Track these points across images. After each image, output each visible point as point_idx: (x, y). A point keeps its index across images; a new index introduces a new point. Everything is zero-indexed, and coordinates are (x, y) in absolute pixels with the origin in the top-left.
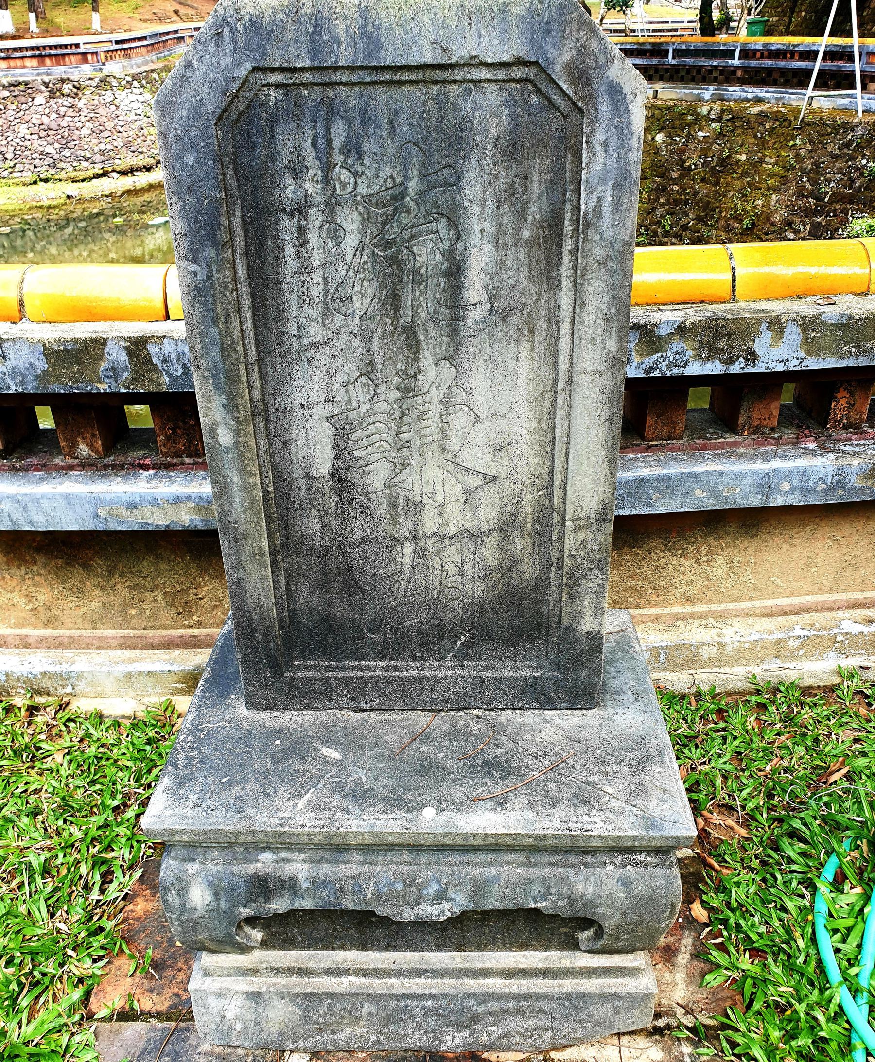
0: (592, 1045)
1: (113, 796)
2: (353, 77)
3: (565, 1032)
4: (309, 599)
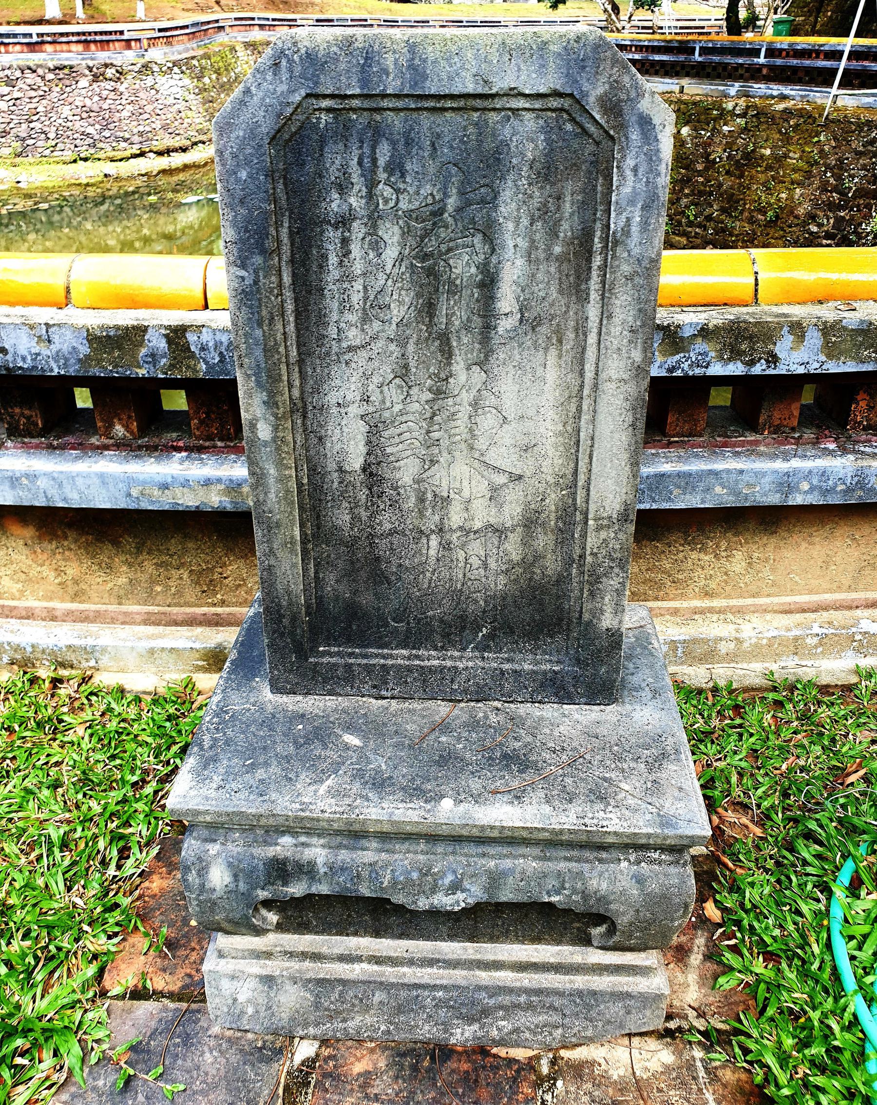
0: (602, 1045)
1: (133, 771)
2: (400, 104)
3: (575, 1030)
4: (336, 586)
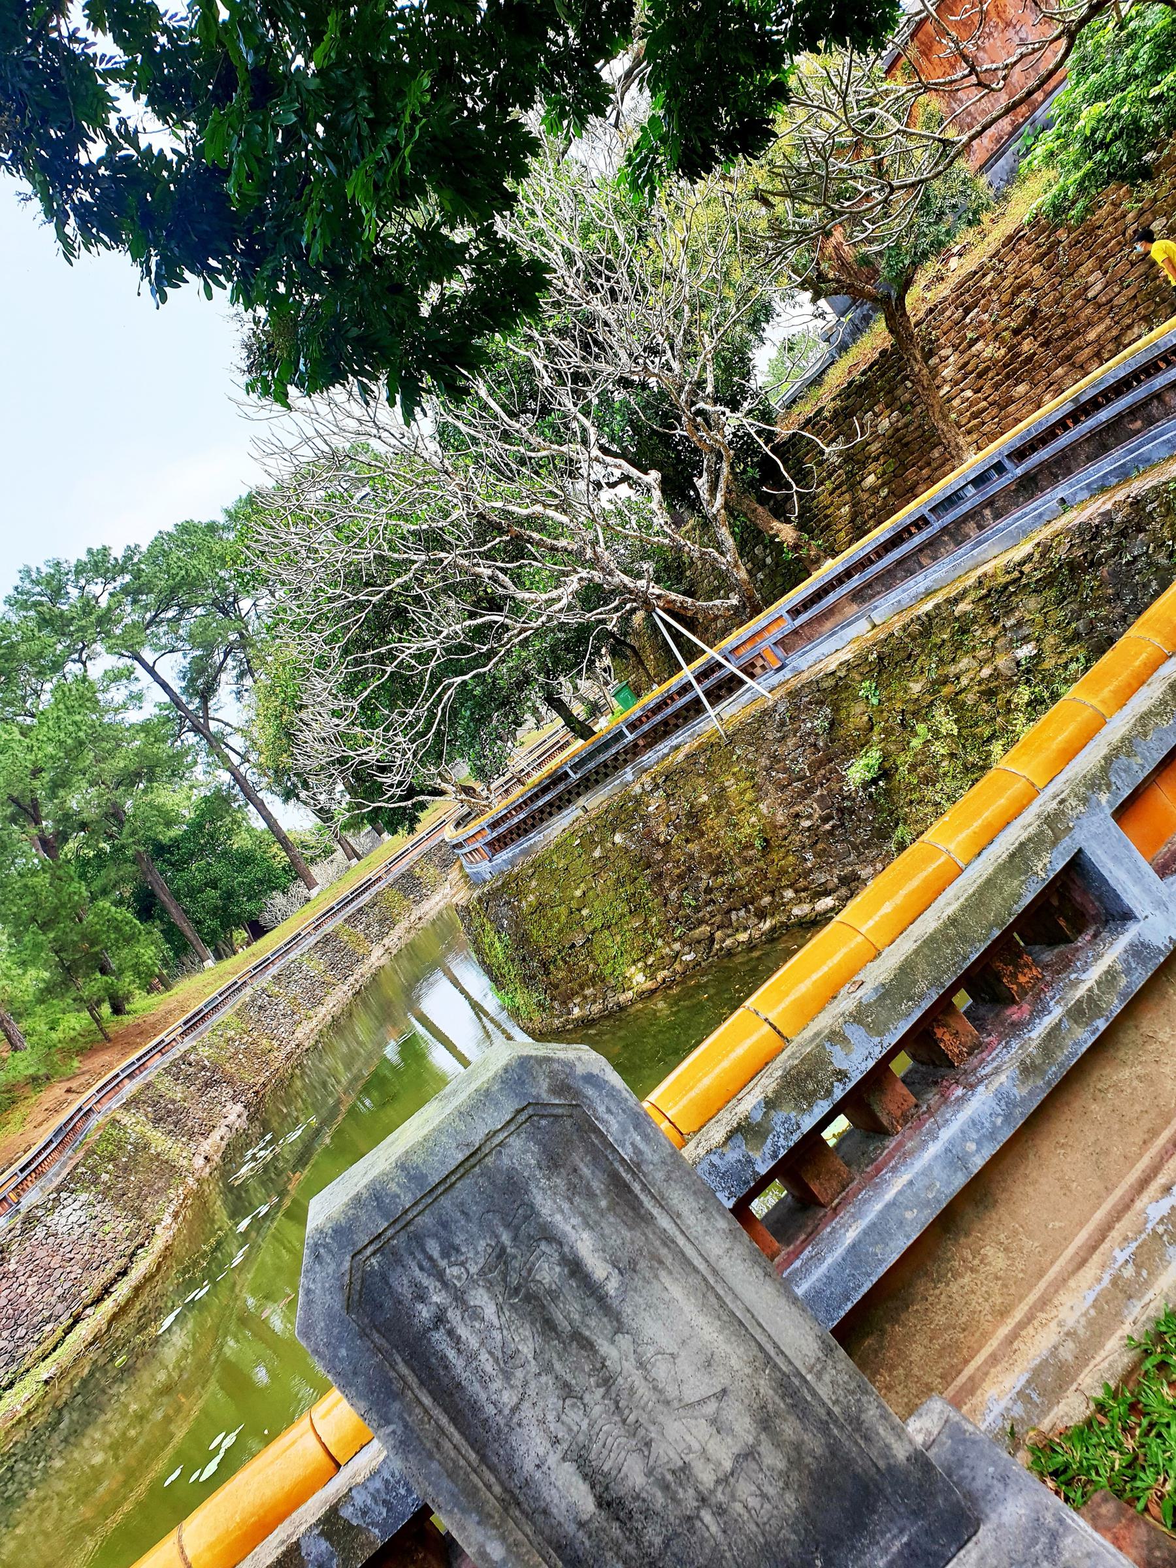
2: (421, 1207)
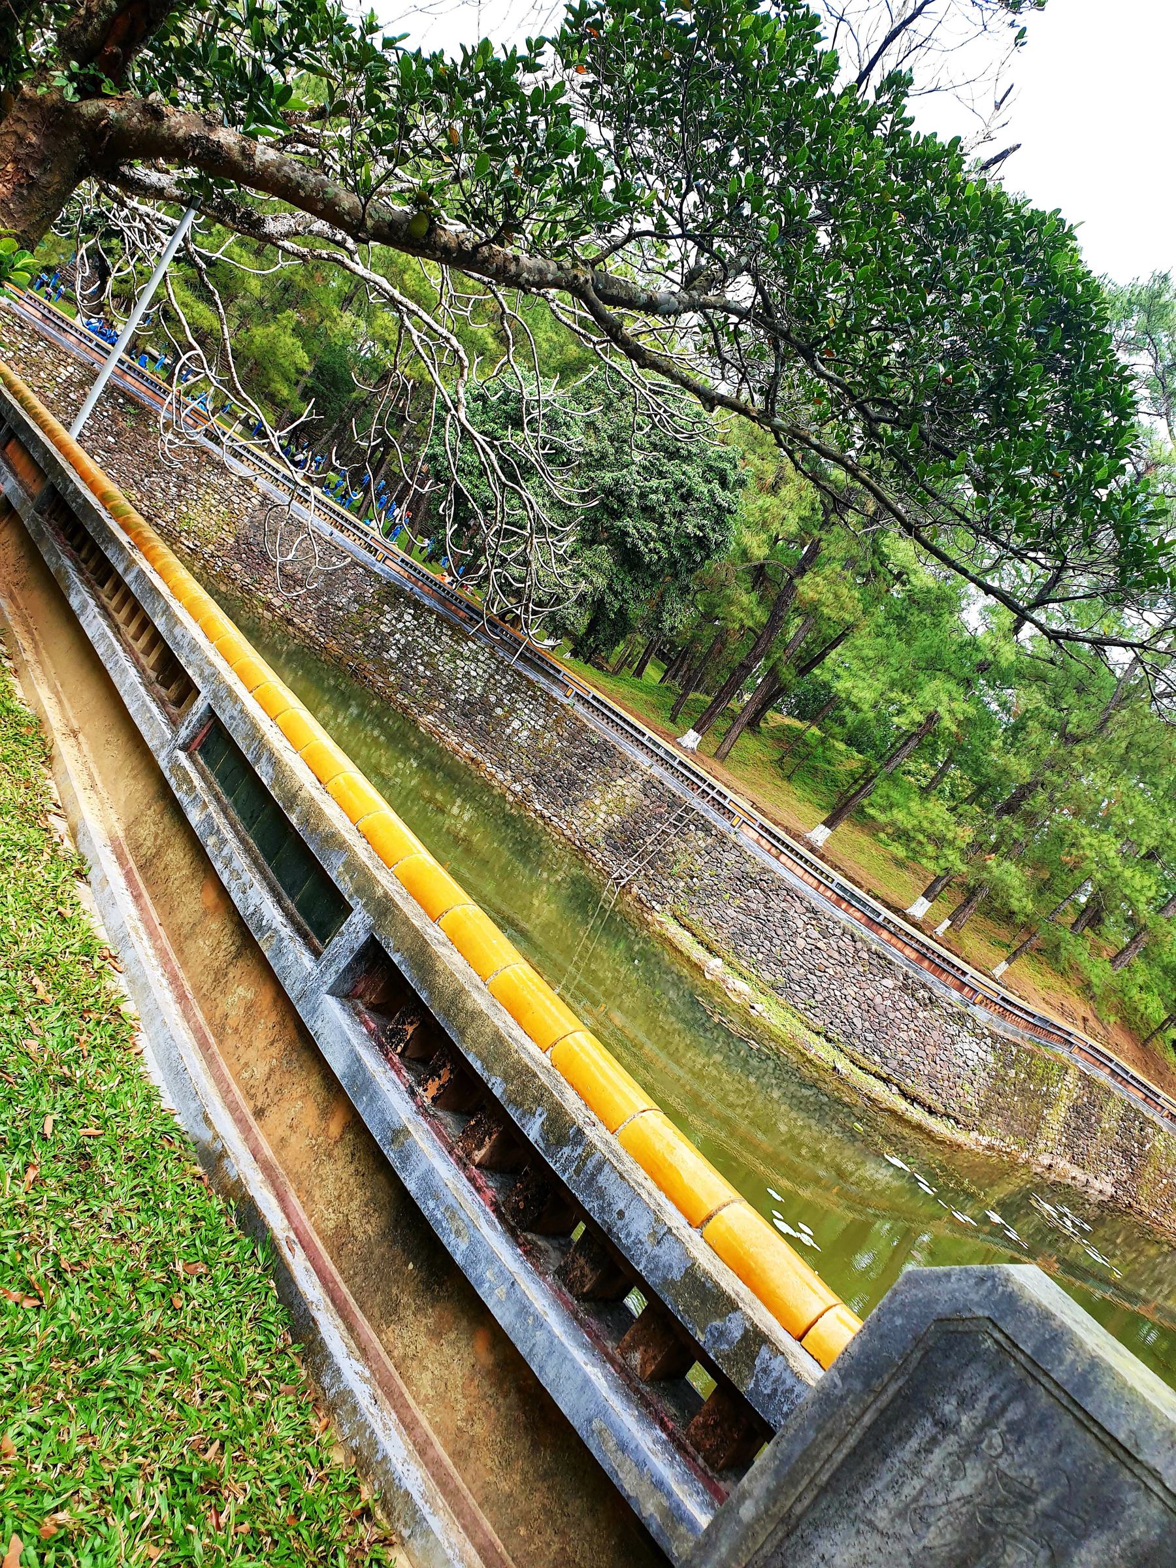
2: (1056, 1392)
